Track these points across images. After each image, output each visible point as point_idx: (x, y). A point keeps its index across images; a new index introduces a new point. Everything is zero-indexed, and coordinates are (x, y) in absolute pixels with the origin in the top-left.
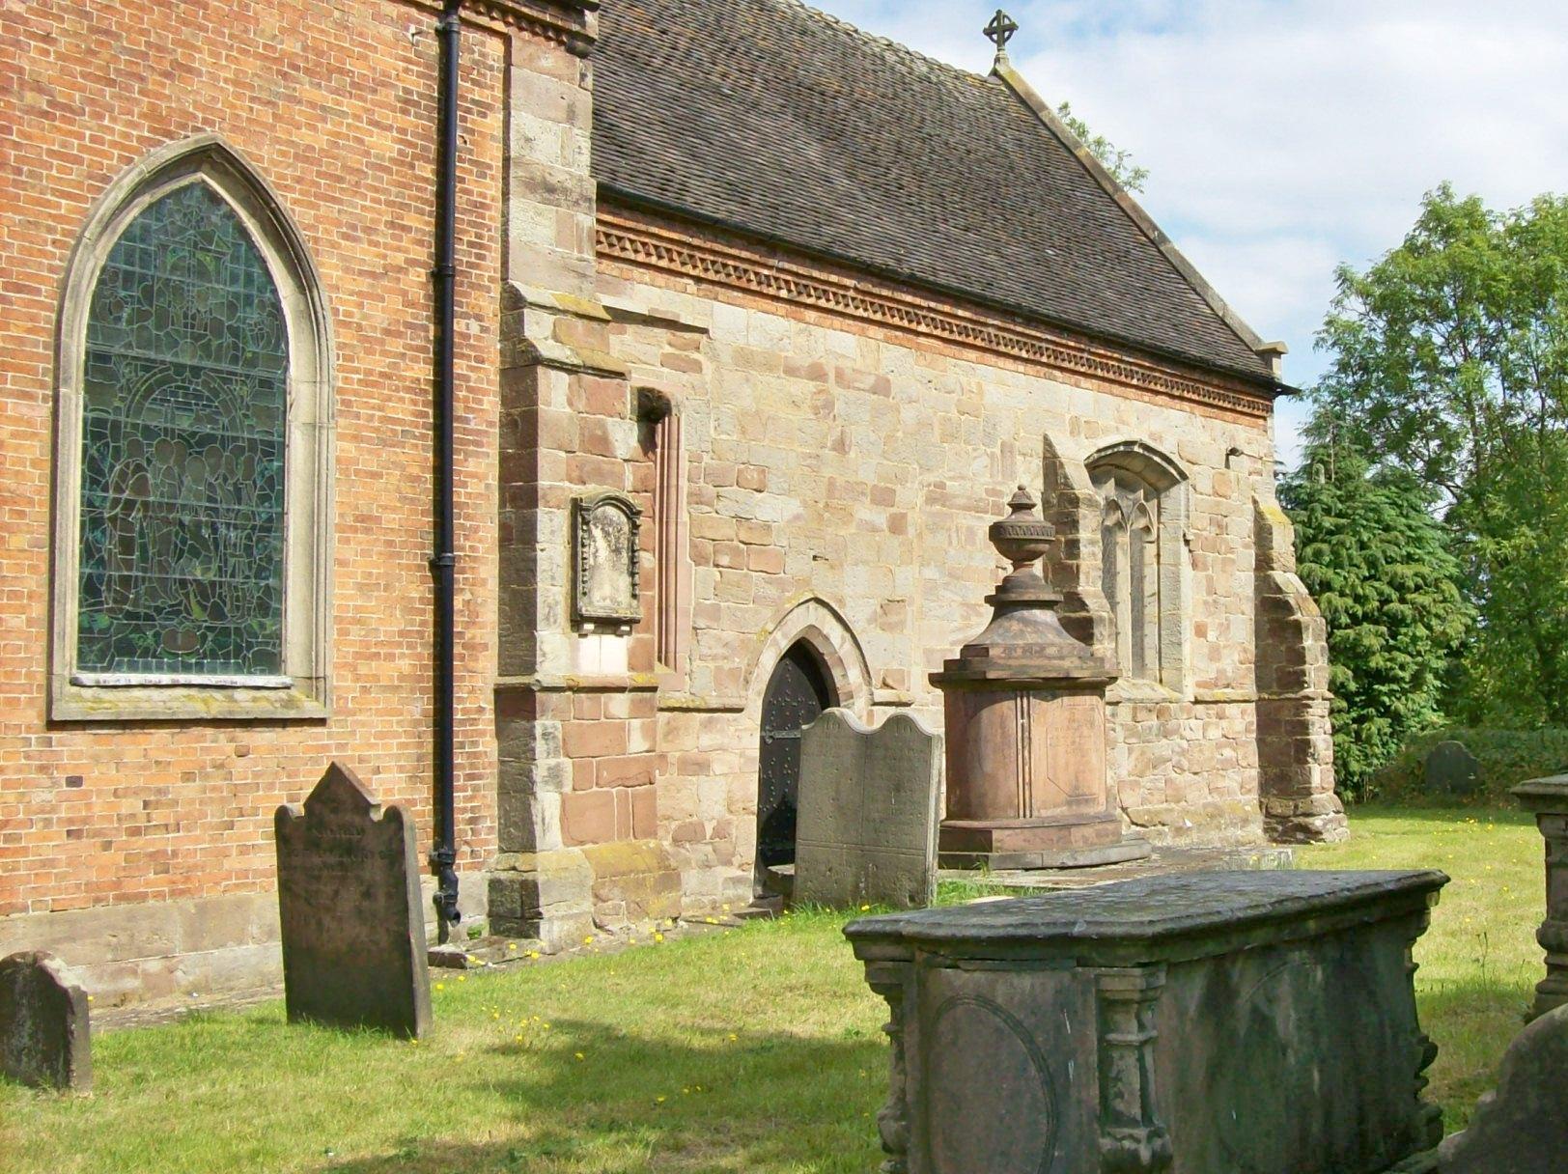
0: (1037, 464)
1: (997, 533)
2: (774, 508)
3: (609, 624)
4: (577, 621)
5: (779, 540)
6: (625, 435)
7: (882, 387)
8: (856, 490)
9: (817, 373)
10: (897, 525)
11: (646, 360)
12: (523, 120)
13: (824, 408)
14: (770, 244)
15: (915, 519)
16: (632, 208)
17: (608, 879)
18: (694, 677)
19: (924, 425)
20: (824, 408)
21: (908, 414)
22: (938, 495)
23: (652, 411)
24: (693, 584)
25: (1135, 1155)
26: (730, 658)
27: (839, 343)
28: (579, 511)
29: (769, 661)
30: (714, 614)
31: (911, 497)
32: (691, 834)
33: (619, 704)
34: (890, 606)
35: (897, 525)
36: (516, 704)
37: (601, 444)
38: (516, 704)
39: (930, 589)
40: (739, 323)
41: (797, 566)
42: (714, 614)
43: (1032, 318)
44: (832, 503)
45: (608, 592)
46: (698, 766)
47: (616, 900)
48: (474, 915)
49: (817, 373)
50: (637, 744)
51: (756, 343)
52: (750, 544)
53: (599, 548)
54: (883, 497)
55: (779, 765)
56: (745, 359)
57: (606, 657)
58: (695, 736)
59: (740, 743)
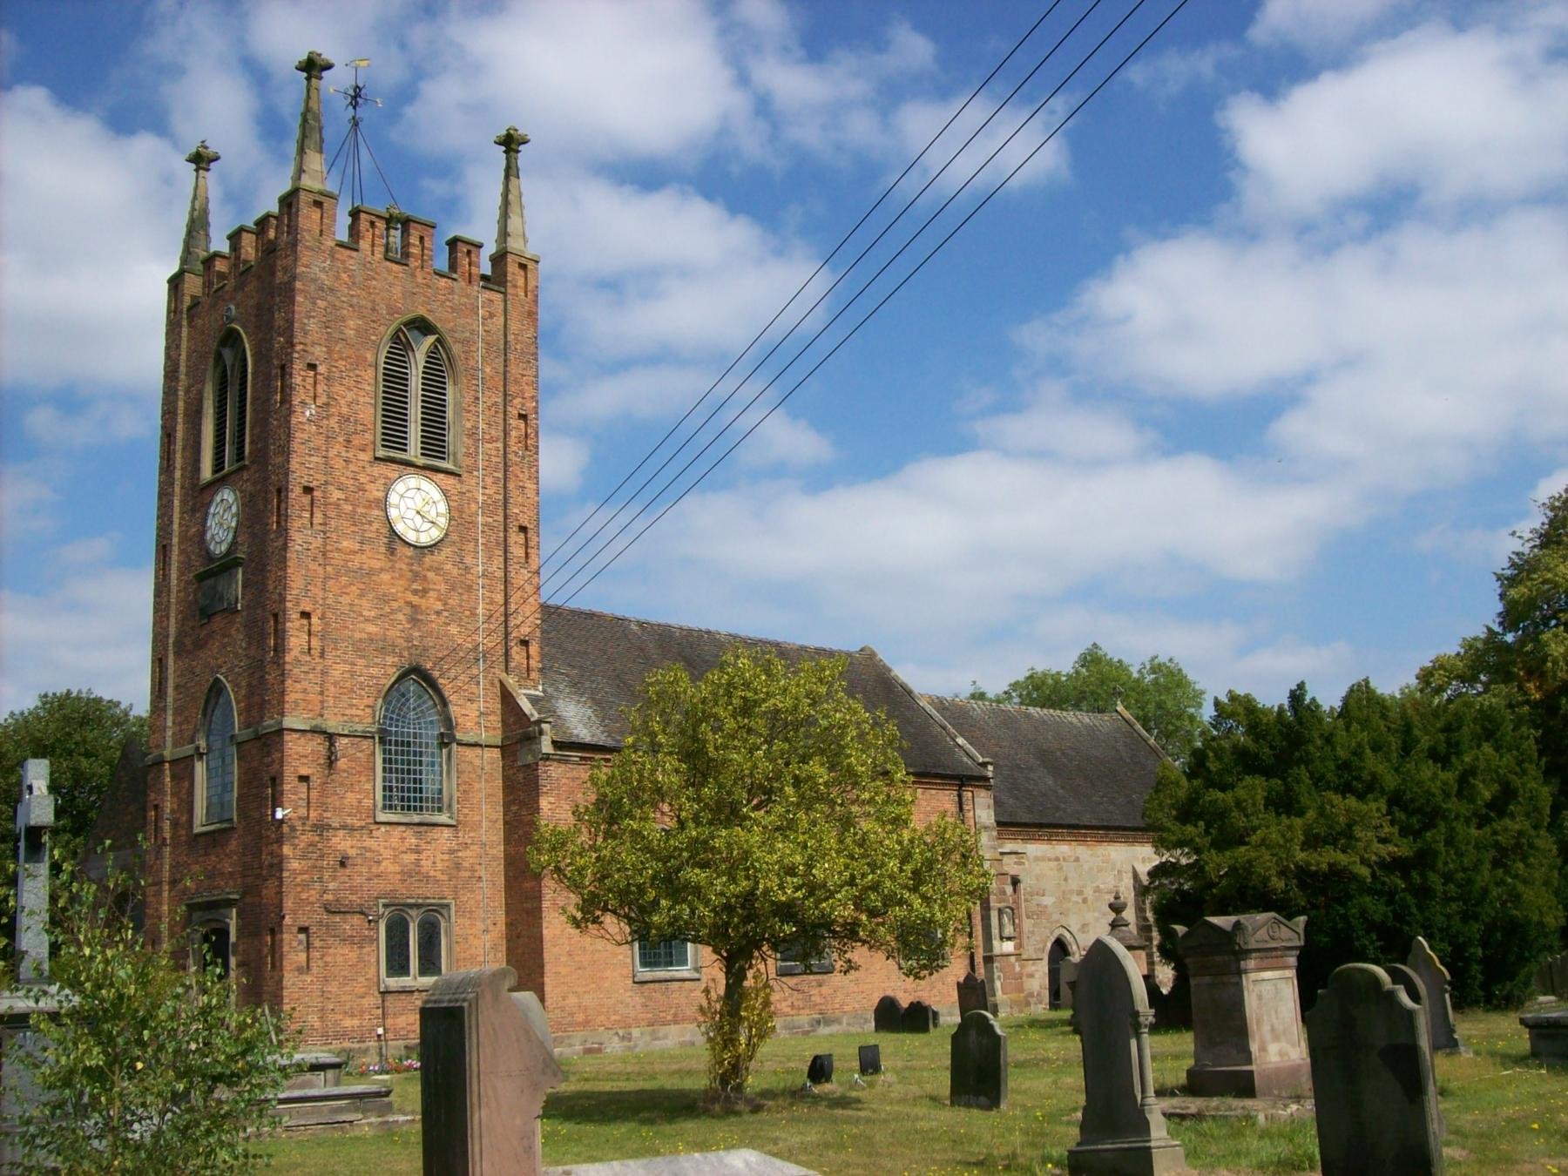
0: (1130, 875)
1: (1111, 906)
2: (1048, 900)
3: (1009, 939)
4: (1002, 938)
5: (1050, 910)
6: (1009, 889)
7: (1077, 860)
8: (1071, 892)
9: (1057, 859)
10: (1085, 901)
11: (1010, 866)
12: (978, 812)
13: (1060, 869)
14: (1041, 826)
15: (1090, 898)
16: (1007, 825)
17: (1013, 1003)
18: (1029, 951)
19: (1091, 869)
20: (1060, 869)
21: (1086, 866)
22: (1097, 890)
23: (1015, 882)
24: (1027, 925)
25: (277, 802)
26: (1039, 943)
27: (1064, 849)
28: (1000, 911)
29: (1049, 945)
30: (1033, 933)
31: (1089, 892)
32: (1031, 995)
33: (1013, 959)
34: (1084, 926)
35: (1085, 901)
36: (989, 960)
37: (1004, 893)
38: (989, 960)
39: (1097, 919)
40: (1034, 849)
41: (1055, 917)
42: (1033, 933)
43: (1125, 829)
44: (1064, 897)
45: (1009, 930)
46: (1031, 976)
47: (1016, 1008)
48: (1151, 1092)
49: (1057, 859)
50: (1017, 969)
51: (1039, 854)
52: (1042, 912)
53: (1006, 919)
54: (1080, 893)
55: (1054, 974)
56: (1037, 859)
57: (1009, 947)
58: (1030, 968)
59: (1043, 967)
